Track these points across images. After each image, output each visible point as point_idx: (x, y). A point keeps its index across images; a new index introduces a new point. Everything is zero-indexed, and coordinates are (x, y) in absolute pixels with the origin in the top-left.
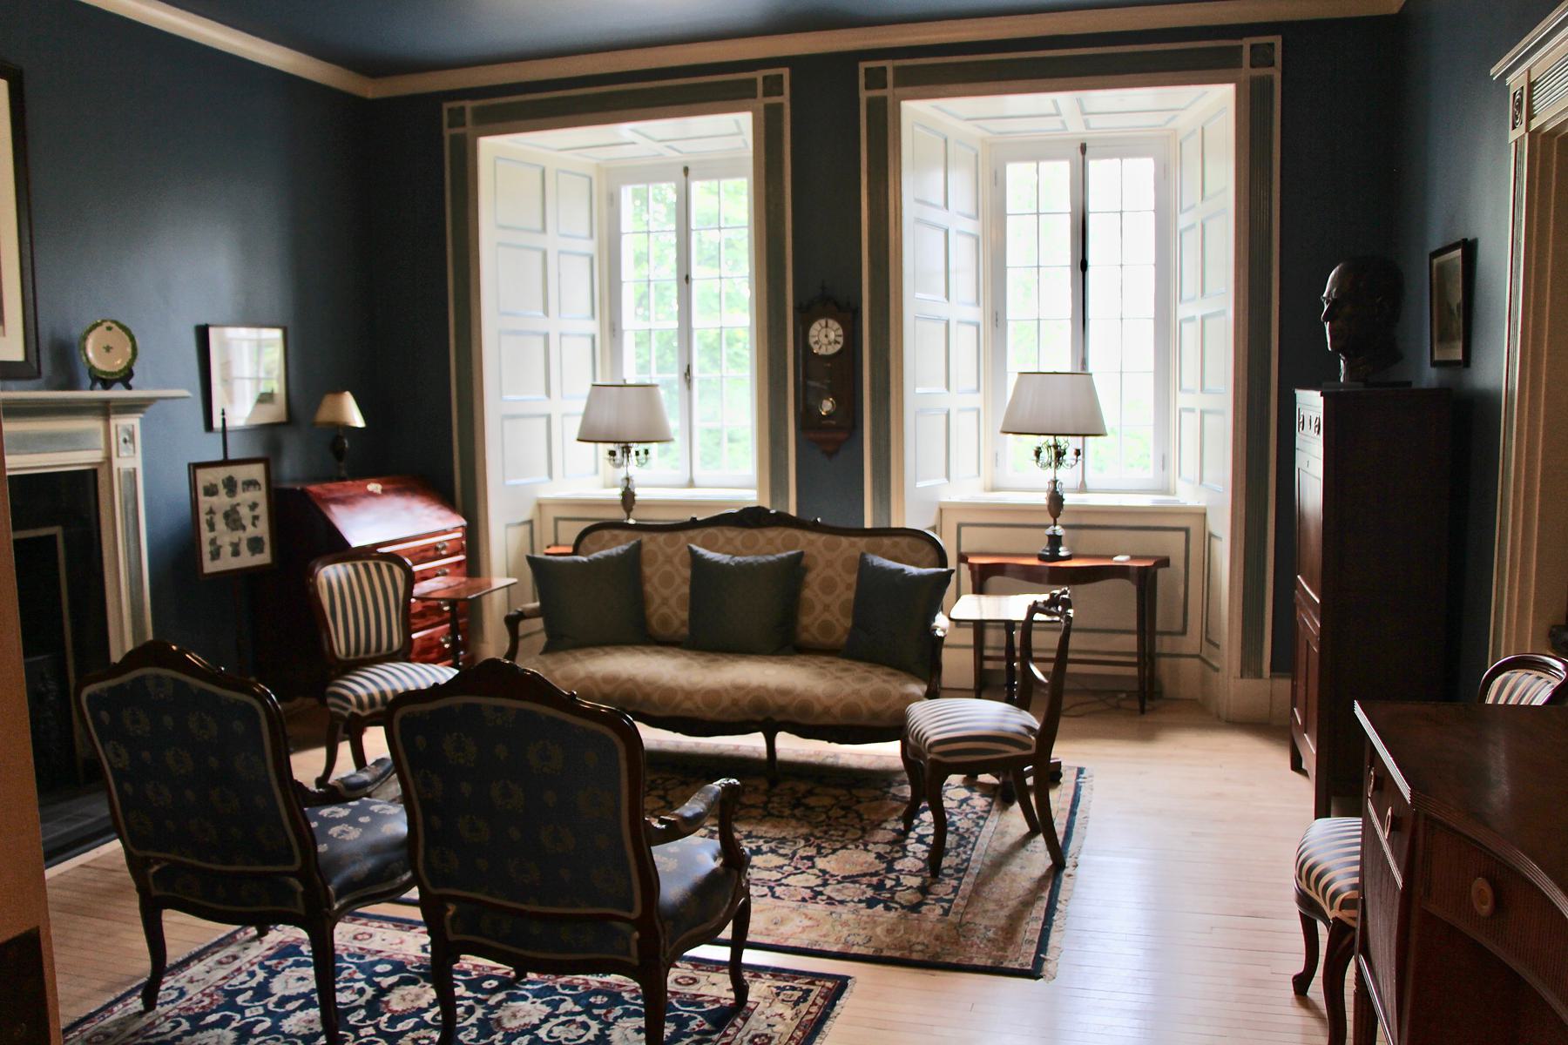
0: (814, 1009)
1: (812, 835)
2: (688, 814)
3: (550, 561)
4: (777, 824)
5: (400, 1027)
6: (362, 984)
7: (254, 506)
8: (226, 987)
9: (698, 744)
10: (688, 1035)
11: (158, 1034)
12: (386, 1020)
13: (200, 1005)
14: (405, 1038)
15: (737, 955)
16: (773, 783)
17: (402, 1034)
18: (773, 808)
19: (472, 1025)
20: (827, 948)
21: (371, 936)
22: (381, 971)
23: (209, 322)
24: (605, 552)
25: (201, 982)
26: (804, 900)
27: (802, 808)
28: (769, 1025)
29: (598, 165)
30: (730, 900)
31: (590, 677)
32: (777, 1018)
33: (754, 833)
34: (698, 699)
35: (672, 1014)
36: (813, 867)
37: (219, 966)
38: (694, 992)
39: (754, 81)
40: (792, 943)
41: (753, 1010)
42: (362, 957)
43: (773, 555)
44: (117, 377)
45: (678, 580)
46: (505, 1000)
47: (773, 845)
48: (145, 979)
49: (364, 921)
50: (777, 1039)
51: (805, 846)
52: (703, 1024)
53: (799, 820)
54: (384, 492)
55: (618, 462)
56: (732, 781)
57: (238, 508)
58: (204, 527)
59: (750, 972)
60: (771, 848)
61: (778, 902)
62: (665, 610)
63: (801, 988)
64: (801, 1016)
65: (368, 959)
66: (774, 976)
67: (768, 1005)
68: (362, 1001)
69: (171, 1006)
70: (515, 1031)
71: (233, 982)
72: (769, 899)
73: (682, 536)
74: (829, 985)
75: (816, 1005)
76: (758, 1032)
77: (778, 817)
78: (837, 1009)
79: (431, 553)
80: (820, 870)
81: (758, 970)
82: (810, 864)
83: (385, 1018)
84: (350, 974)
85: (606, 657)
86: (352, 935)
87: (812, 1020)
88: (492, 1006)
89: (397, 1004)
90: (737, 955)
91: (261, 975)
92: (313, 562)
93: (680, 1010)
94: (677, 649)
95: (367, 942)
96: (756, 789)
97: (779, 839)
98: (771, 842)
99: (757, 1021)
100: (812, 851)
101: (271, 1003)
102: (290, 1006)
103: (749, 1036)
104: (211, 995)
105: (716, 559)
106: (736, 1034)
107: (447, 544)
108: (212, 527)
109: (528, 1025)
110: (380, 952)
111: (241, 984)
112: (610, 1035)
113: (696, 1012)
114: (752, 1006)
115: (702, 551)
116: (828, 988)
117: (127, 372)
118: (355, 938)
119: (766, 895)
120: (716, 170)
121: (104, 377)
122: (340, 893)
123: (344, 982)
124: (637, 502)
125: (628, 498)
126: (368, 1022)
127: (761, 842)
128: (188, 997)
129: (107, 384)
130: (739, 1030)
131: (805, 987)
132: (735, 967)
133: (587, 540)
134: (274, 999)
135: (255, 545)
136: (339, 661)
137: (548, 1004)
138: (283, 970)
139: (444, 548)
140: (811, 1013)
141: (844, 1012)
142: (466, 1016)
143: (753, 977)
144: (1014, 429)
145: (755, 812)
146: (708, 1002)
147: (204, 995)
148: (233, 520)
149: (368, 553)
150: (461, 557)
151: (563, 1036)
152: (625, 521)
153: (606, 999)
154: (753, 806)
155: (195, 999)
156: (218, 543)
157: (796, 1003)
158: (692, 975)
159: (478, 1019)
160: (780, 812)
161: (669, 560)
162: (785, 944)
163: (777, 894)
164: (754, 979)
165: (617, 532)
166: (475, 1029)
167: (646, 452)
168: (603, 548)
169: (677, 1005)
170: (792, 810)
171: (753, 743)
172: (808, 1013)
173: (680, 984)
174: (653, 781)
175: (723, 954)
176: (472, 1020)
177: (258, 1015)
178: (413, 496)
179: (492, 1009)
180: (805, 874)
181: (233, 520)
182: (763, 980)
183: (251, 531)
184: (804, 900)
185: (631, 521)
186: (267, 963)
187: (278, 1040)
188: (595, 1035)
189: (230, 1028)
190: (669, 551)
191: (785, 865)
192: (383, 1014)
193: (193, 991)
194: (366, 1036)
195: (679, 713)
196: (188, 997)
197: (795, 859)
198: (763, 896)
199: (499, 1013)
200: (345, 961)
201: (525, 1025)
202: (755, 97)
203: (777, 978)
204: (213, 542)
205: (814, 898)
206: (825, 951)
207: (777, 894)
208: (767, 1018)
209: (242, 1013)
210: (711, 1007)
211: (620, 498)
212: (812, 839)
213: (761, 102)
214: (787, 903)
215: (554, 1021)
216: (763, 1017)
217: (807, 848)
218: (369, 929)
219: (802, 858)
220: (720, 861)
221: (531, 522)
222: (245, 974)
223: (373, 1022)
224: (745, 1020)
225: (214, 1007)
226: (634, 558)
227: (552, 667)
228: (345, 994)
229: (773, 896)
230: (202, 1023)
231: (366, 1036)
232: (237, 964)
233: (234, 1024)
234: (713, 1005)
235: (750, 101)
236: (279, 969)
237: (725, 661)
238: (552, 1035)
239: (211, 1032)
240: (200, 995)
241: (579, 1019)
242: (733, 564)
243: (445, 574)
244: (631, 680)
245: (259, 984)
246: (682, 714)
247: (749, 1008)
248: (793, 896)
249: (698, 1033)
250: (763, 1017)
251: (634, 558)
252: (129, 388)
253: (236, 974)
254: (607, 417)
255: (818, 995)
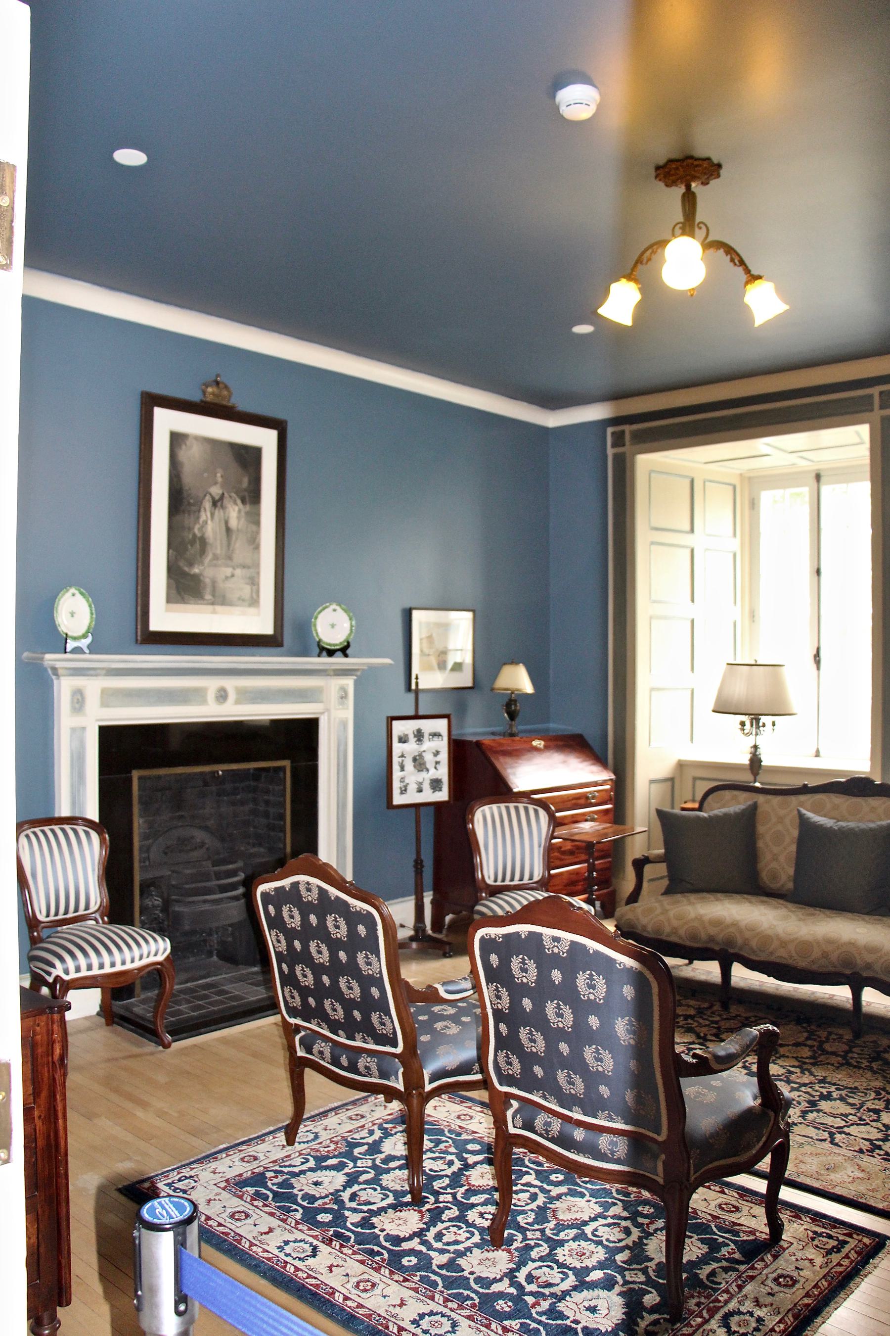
0: (846, 1262)
1: (884, 1089)
2: (722, 1053)
3: (683, 817)
4: (852, 1073)
5: (473, 1200)
6: (453, 1157)
7: (437, 753)
8: (349, 1139)
9: (796, 990)
10: (718, 1260)
11: (290, 1166)
12: (463, 1191)
13: (326, 1150)
14: (474, 1210)
15: (773, 1190)
16: (857, 1035)
17: (473, 1206)
18: (852, 1058)
19: (532, 1210)
20: (872, 1203)
21: (471, 1117)
22: (471, 1149)
23: (413, 606)
24: (724, 810)
25: (332, 1131)
26: (861, 1151)
27: (880, 1062)
28: (797, 1268)
29: (741, 475)
30: (764, 1139)
31: (699, 919)
32: (807, 1263)
33: (828, 1080)
34: (791, 947)
35: (708, 1236)
36: (877, 1121)
37: (349, 1121)
38: (734, 1220)
39: (871, 396)
40: (838, 1191)
41: (784, 1250)
42: (459, 1134)
43: (873, 822)
44: (338, 647)
45: (787, 840)
46: (566, 1194)
47: (844, 1093)
48: (287, 1122)
49: (469, 1104)
50: (801, 1283)
51: (874, 1099)
52: (734, 1253)
53: (874, 1072)
54: (547, 747)
55: (746, 732)
56: (771, 1027)
57: (424, 754)
58: (396, 767)
59: (791, 1212)
60: (841, 1095)
61: (836, 1150)
62: (774, 865)
63: (837, 1237)
64: (831, 1265)
65: (464, 1137)
66: (813, 1220)
67: (801, 1247)
68: (449, 1172)
69: (306, 1145)
70: (566, 1223)
71: (356, 1136)
72: (827, 1145)
73: (794, 800)
74: (866, 1241)
75: (849, 1258)
76: (784, 1272)
77: (855, 1067)
78: (869, 1267)
79: (582, 801)
80: (884, 1125)
81: (799, 1211)
82: (875, 1117)
83: (463, 1190)
84: (445, 1147)
85: (717, 903)
86: (457, 1114)
87: (841, 1273)
88: (554, 1197)
89: (476, 1179)
90: (773, 1190)
91: (378, 1134)
92: (472, 803)
93: (716, 1234)
94: (781, 901)
95: (469, 1122)
96: (841, 1037)
97: (851, 1088)
98: (843, 1090)
99: (787, 1261)
100: (880, 1105)
101: (379, 1158)
102: (392, 1165)
103: (775, 1275)
104: (337, 1143)
105: (822, 823)
106: (763, 1269)
107: (597, 794)
108: (402, 768)
109: (578, 1220)
110: (476, 1133)
111: (361, 1138)
112: (646, 1245)
113: (731, 1240)
114: (785, 1245)
115: (809, 814)
116: (865, 1244)
117: (346, 644)
118: (459, 1117)
119: (825, 1140)
120: (844, 474)
121: (329, 647)
122: (434, 1078)
123: (440, 1153)
124: (762, 768)
125: (755, 762)
126: (449, 1190)
127: (833, 1088)
128: (319, 1141)
129: (331, 653)
130: (766, 1266)
131: (841, 1237)
132: (771, 1202)
133: (710, 797)
134: (382, 1156)
135: (436, 784)
136: (488, 886)
137: (601, 1204)
138: (396, 1134)
139: (593, 798)
140: (842, 1265)
141: (877, 1272)
142: (529, 1201)
143: (793, 1216)
144: (722, 708)
145: (834, 1060)
146: (744, 1232)
147: (332, 1142)
148: (419, 763)
149: (526, 796)
150: (609, 806)
151: (606, 1237)
152: (751, 784)
153: (652, 1210)
154: (834, 1053)
155: (324, 1144)
156: (407, 781)
157: (829, 1252)
158: (735, 1203)
159: (538, 1207)
160: (857, 1062)
161: (781, 820)
162: (832, 1191)
163: (837, 1141)
164: (794, 1219)
165: (736, 793)
166: (533, 1214)
167: (774, 724)
168: (723, 807)
169: (715, 1229)
170: (870, 1062)
171: (842, 994)
172: (839, 1264)
173: (723, 1209)
174: (747, 1018)
175: (761, 1186)
176: (534, 1206)
177: (366, 1167)
178: (571, 752)
179: (552, 1199)
180: (868, 1126)
181: (419, 763)
182: (802, 1222)
183: (433, 774)
184: (861, 1151)
185: (757, 785)
186: (385, 1126)
187: (375, 1190)
188: (634, 1241)
189: (343, 1172)
190: (782, 812)
191: (851, 1114)
192: (462, 1186)
193: (324, 1136)
194: (444, 1202)
195: (772, 959)
196: (319, 1141)
197: (861, 1110)
198: (821, 1140)
199: (558, 1204)
200: (445, 1135)
201: (576, 1219)
202: (872, 410)
203: (817, 1223)
204: (402, 780)
205: (872, 1151)
206: (871, 1206)
207: (837, 1141)
208: (797, 1260)
209: (355, 1162)
210: (745, 1238)
211: (747, 762)
212: (883, 1093)
213: (878, 414)
214: (843, 1151)
215: (602, 1221)
216: (793, 1258)
217: (876, 1102)
218: (471, 1112)
219: (869, 1110)
220: (759, 1101)
221: (671, 780)
222: (366, 1131)
223: (452, 1191)
224: (775, 1257)
225: (336, 1153)
226: (750, 816)
227: (668, 907)
228: (437, 1163)
229: (832, 1142)
230: (324, 1164)
231: (444, 1202)
232: (362, 1122)
233: (346, 1170)
234: (748, 1236)
235: (866, 415)
236: (393, 1132)
237: (822, 915)
238: (596, 1233)
239: (328, 1173)
240: (328, 1141)
241: (624, 1223)
242: (836, 828)
243: (593, 820)
244: (735, 924)
245: (375, 1141)
246: (778, 961)
247: (781, 1247)
248: (852, 1146)
249: (727, 1260)
250: (793, 1258)
251: (750, 816)
252: (346, 656)
253: (360, 1129)
254: (739, 690)
255: (852, 1249)
